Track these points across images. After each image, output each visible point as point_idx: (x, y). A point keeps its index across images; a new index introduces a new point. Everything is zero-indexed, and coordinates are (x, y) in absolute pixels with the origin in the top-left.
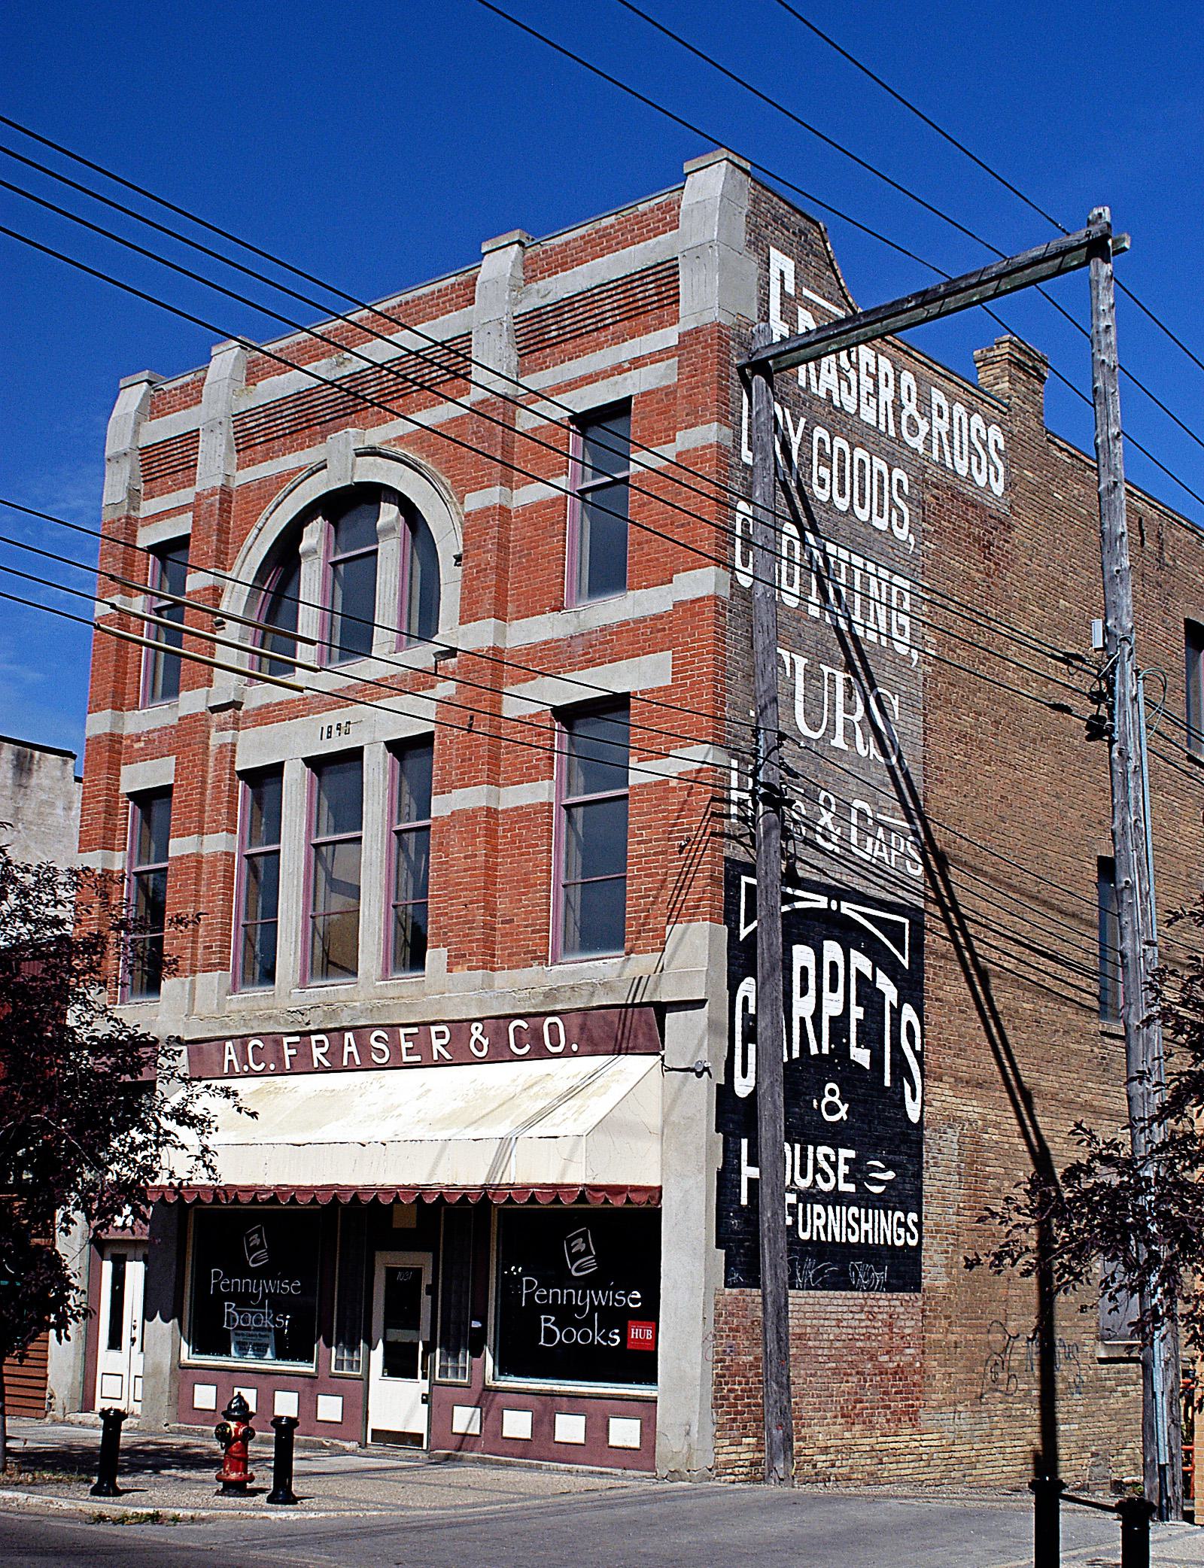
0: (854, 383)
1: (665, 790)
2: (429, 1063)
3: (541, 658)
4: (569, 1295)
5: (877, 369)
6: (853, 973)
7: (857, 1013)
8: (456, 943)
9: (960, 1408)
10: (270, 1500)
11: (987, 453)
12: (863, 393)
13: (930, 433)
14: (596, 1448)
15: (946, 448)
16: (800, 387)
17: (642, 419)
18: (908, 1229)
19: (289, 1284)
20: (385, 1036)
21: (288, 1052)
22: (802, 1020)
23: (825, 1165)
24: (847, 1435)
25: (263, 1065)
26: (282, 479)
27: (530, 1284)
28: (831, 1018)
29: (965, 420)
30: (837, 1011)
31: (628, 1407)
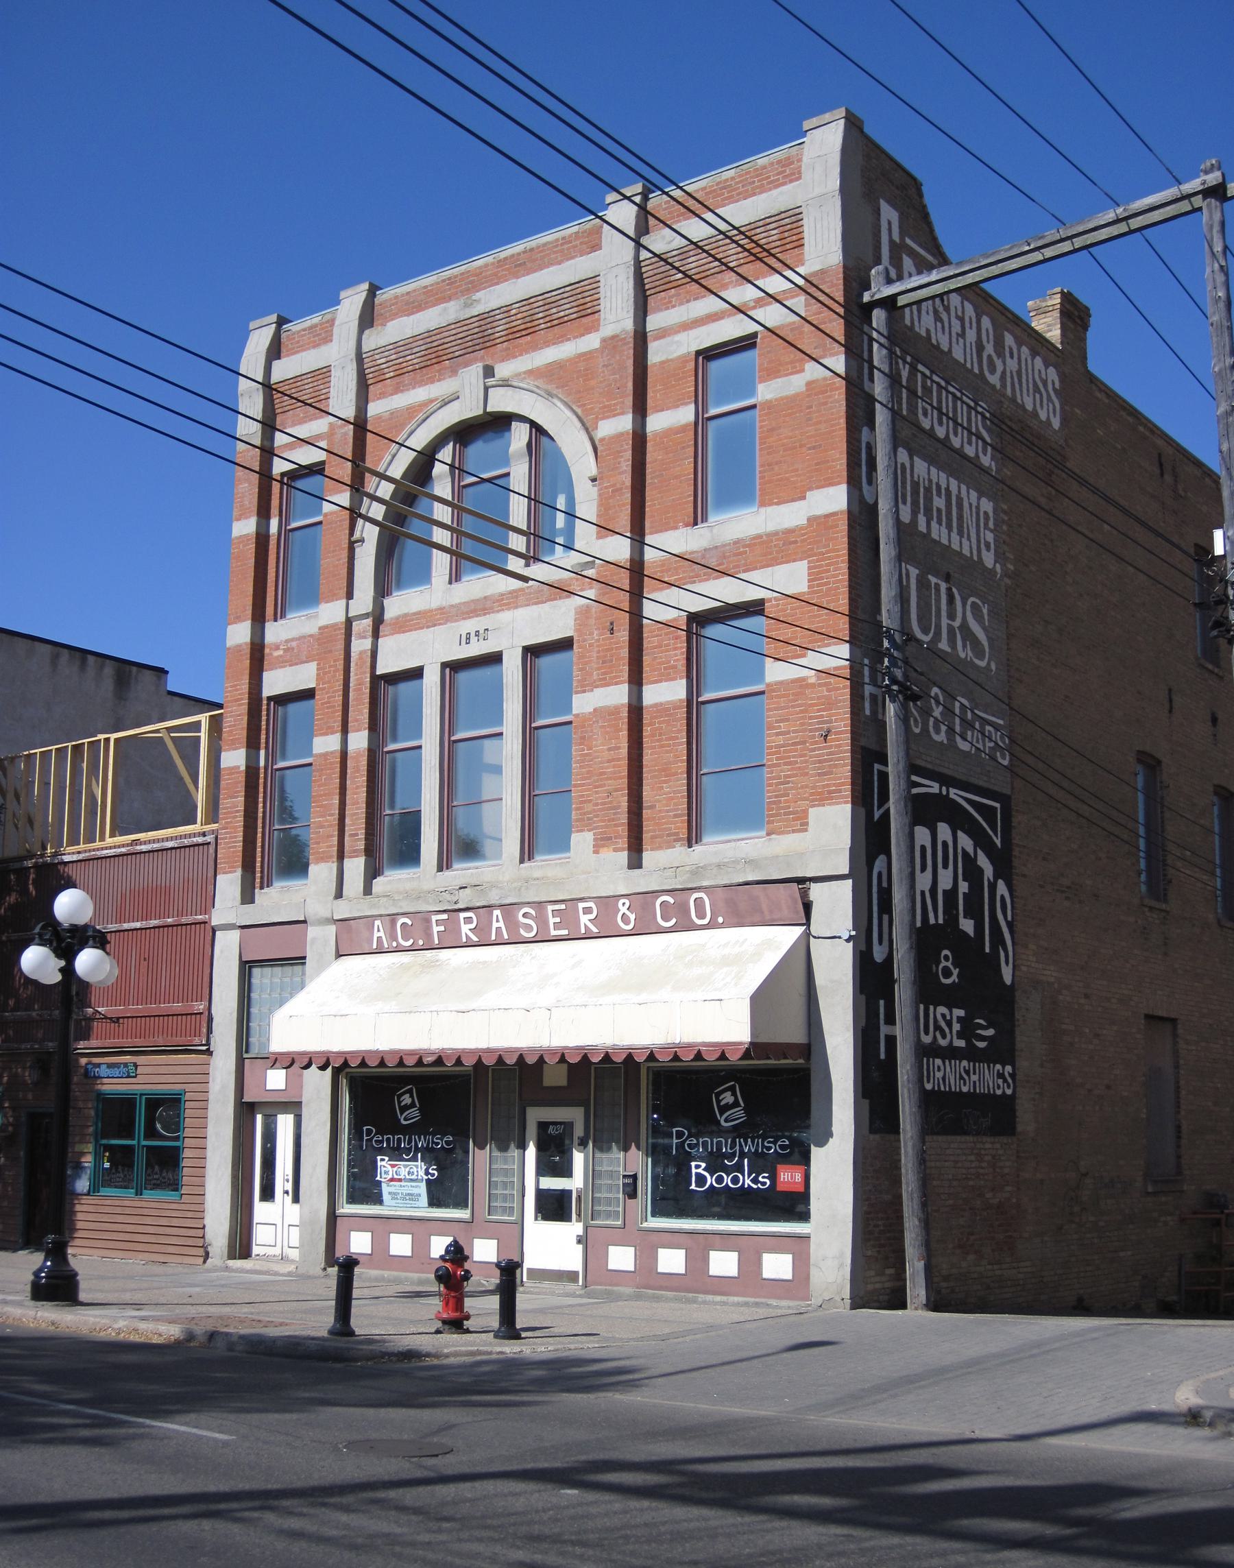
0: (946, 325)
1: (801, 686)
2: (543, 939)
3: (676, 569)
4: (719, 1143)
5: (963, 312)
6: (960, 850)
7: (964, 887)
8: (602, 827)
9: (1046, 1238)
10: (496, 1337)
11: (1047, 391)
12: (954, 335)
13: (1004, 372)
14: (696, 1279)
15: (1017, 386)
16: (906, 326)
17: (769, 352)
18: (1005, 1081)
19: (775, 1143)
20: (533, 912)
21: (436, 929)
22: (923, 893)
23: (943, 1024)
24: (964, 1264)
25: (411, 941)
26: (412, 411)
27: (369, 1132)
28: (944, 891)
29: (1030, 362)
30: (949, 887)
31: (779, 1243)
